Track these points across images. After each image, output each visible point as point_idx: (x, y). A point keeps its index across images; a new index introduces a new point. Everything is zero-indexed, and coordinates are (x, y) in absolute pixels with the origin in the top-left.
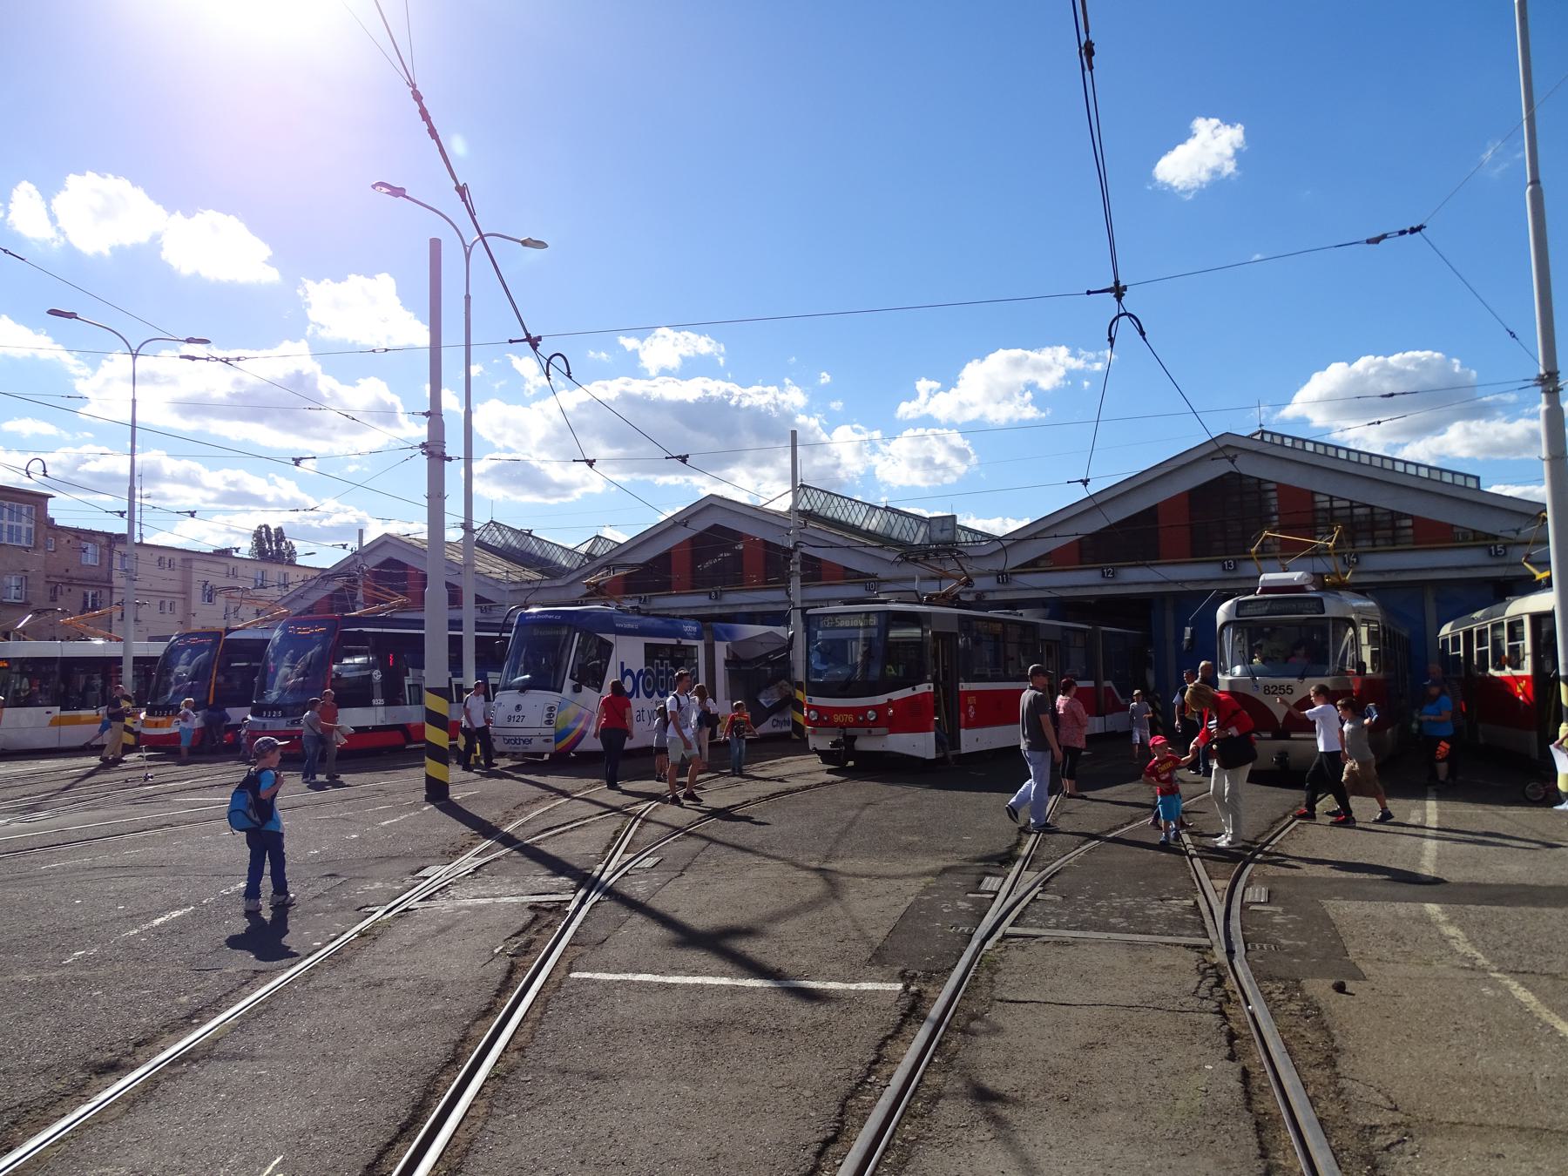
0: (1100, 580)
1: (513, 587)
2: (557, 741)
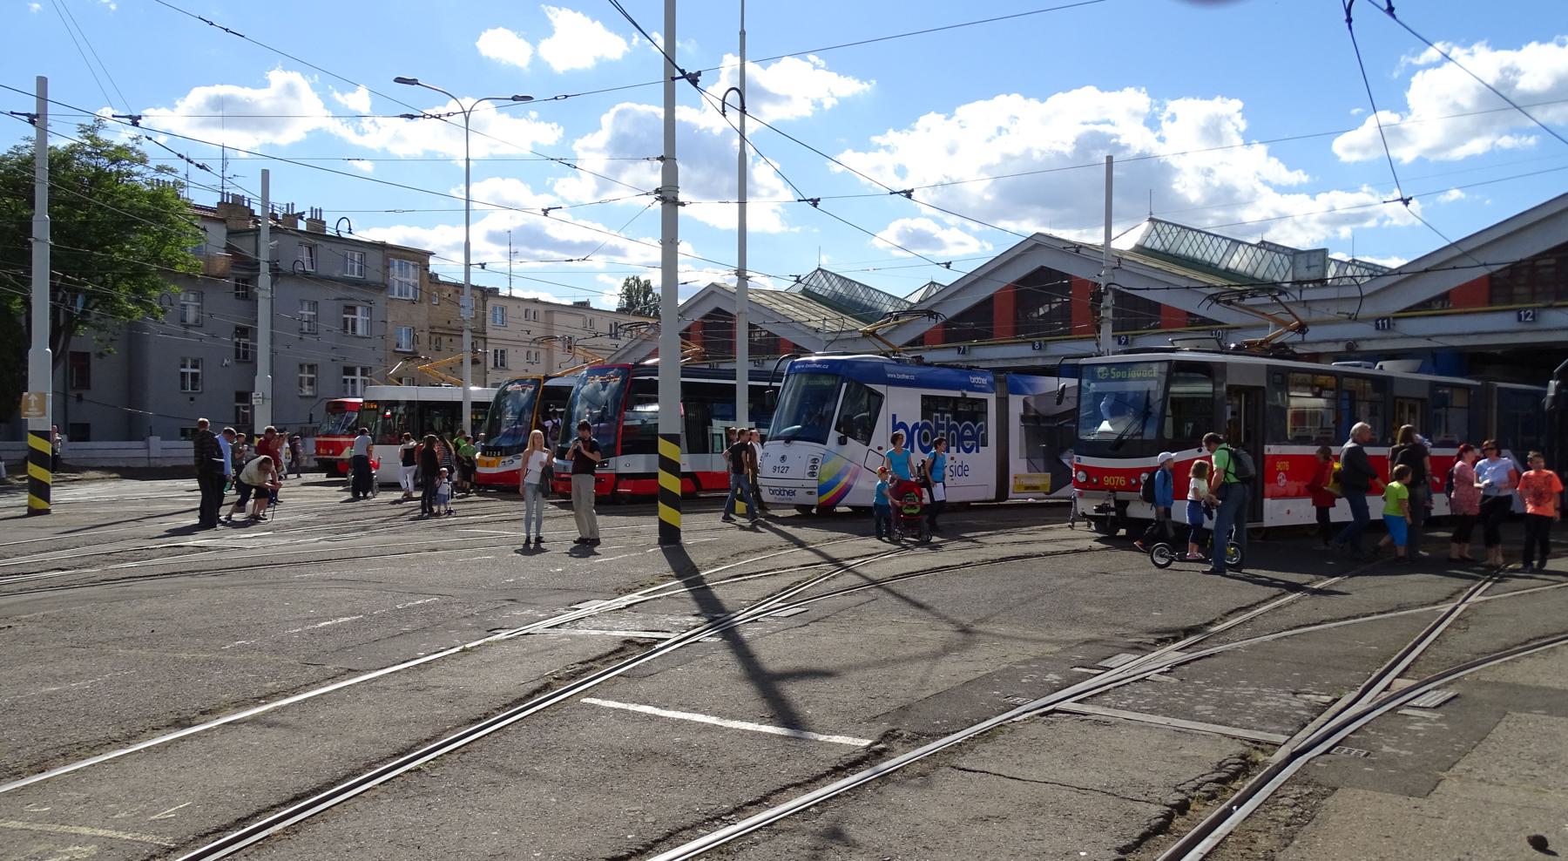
0: (1517, 326)
1: (831, 337)
2: (820, 494)
